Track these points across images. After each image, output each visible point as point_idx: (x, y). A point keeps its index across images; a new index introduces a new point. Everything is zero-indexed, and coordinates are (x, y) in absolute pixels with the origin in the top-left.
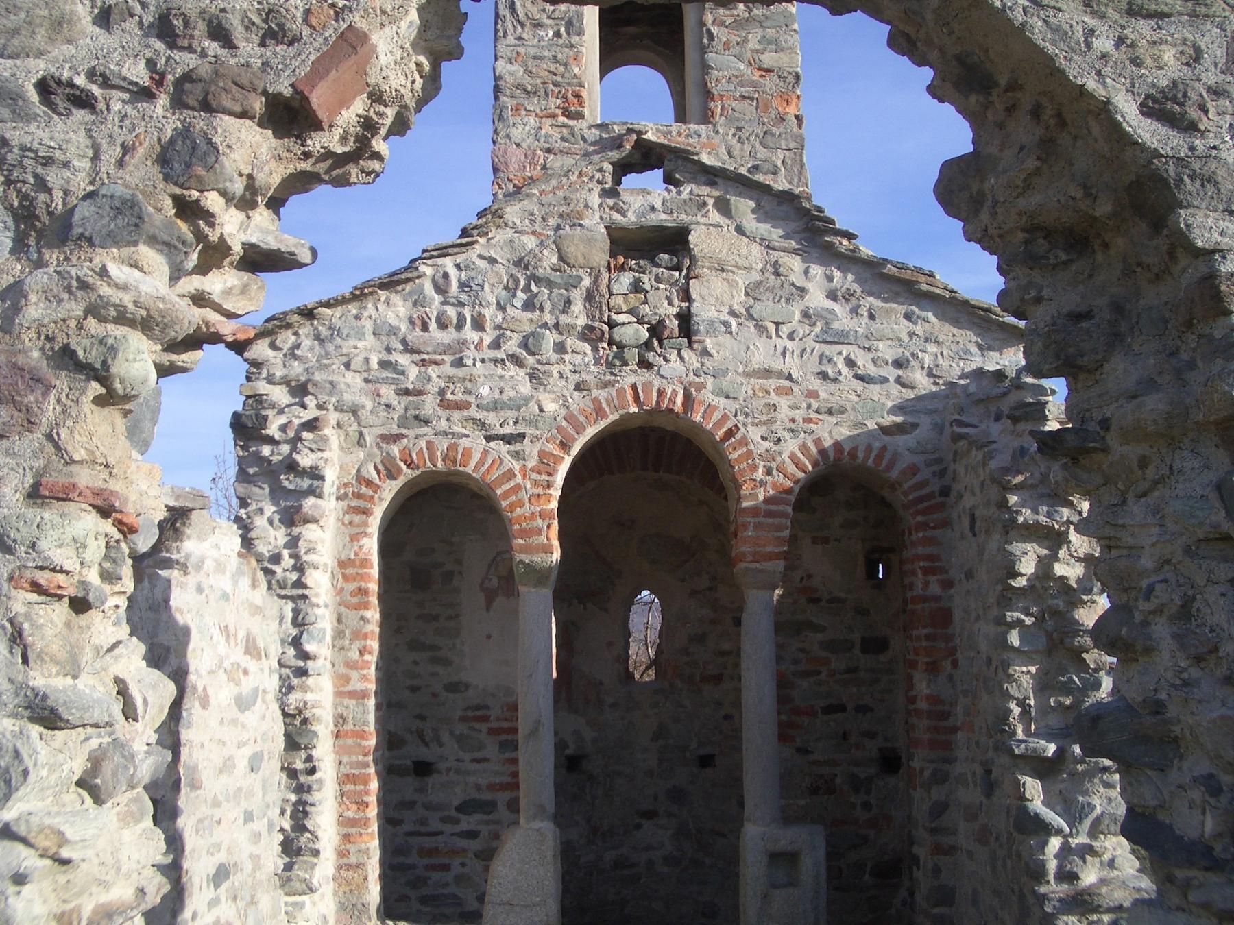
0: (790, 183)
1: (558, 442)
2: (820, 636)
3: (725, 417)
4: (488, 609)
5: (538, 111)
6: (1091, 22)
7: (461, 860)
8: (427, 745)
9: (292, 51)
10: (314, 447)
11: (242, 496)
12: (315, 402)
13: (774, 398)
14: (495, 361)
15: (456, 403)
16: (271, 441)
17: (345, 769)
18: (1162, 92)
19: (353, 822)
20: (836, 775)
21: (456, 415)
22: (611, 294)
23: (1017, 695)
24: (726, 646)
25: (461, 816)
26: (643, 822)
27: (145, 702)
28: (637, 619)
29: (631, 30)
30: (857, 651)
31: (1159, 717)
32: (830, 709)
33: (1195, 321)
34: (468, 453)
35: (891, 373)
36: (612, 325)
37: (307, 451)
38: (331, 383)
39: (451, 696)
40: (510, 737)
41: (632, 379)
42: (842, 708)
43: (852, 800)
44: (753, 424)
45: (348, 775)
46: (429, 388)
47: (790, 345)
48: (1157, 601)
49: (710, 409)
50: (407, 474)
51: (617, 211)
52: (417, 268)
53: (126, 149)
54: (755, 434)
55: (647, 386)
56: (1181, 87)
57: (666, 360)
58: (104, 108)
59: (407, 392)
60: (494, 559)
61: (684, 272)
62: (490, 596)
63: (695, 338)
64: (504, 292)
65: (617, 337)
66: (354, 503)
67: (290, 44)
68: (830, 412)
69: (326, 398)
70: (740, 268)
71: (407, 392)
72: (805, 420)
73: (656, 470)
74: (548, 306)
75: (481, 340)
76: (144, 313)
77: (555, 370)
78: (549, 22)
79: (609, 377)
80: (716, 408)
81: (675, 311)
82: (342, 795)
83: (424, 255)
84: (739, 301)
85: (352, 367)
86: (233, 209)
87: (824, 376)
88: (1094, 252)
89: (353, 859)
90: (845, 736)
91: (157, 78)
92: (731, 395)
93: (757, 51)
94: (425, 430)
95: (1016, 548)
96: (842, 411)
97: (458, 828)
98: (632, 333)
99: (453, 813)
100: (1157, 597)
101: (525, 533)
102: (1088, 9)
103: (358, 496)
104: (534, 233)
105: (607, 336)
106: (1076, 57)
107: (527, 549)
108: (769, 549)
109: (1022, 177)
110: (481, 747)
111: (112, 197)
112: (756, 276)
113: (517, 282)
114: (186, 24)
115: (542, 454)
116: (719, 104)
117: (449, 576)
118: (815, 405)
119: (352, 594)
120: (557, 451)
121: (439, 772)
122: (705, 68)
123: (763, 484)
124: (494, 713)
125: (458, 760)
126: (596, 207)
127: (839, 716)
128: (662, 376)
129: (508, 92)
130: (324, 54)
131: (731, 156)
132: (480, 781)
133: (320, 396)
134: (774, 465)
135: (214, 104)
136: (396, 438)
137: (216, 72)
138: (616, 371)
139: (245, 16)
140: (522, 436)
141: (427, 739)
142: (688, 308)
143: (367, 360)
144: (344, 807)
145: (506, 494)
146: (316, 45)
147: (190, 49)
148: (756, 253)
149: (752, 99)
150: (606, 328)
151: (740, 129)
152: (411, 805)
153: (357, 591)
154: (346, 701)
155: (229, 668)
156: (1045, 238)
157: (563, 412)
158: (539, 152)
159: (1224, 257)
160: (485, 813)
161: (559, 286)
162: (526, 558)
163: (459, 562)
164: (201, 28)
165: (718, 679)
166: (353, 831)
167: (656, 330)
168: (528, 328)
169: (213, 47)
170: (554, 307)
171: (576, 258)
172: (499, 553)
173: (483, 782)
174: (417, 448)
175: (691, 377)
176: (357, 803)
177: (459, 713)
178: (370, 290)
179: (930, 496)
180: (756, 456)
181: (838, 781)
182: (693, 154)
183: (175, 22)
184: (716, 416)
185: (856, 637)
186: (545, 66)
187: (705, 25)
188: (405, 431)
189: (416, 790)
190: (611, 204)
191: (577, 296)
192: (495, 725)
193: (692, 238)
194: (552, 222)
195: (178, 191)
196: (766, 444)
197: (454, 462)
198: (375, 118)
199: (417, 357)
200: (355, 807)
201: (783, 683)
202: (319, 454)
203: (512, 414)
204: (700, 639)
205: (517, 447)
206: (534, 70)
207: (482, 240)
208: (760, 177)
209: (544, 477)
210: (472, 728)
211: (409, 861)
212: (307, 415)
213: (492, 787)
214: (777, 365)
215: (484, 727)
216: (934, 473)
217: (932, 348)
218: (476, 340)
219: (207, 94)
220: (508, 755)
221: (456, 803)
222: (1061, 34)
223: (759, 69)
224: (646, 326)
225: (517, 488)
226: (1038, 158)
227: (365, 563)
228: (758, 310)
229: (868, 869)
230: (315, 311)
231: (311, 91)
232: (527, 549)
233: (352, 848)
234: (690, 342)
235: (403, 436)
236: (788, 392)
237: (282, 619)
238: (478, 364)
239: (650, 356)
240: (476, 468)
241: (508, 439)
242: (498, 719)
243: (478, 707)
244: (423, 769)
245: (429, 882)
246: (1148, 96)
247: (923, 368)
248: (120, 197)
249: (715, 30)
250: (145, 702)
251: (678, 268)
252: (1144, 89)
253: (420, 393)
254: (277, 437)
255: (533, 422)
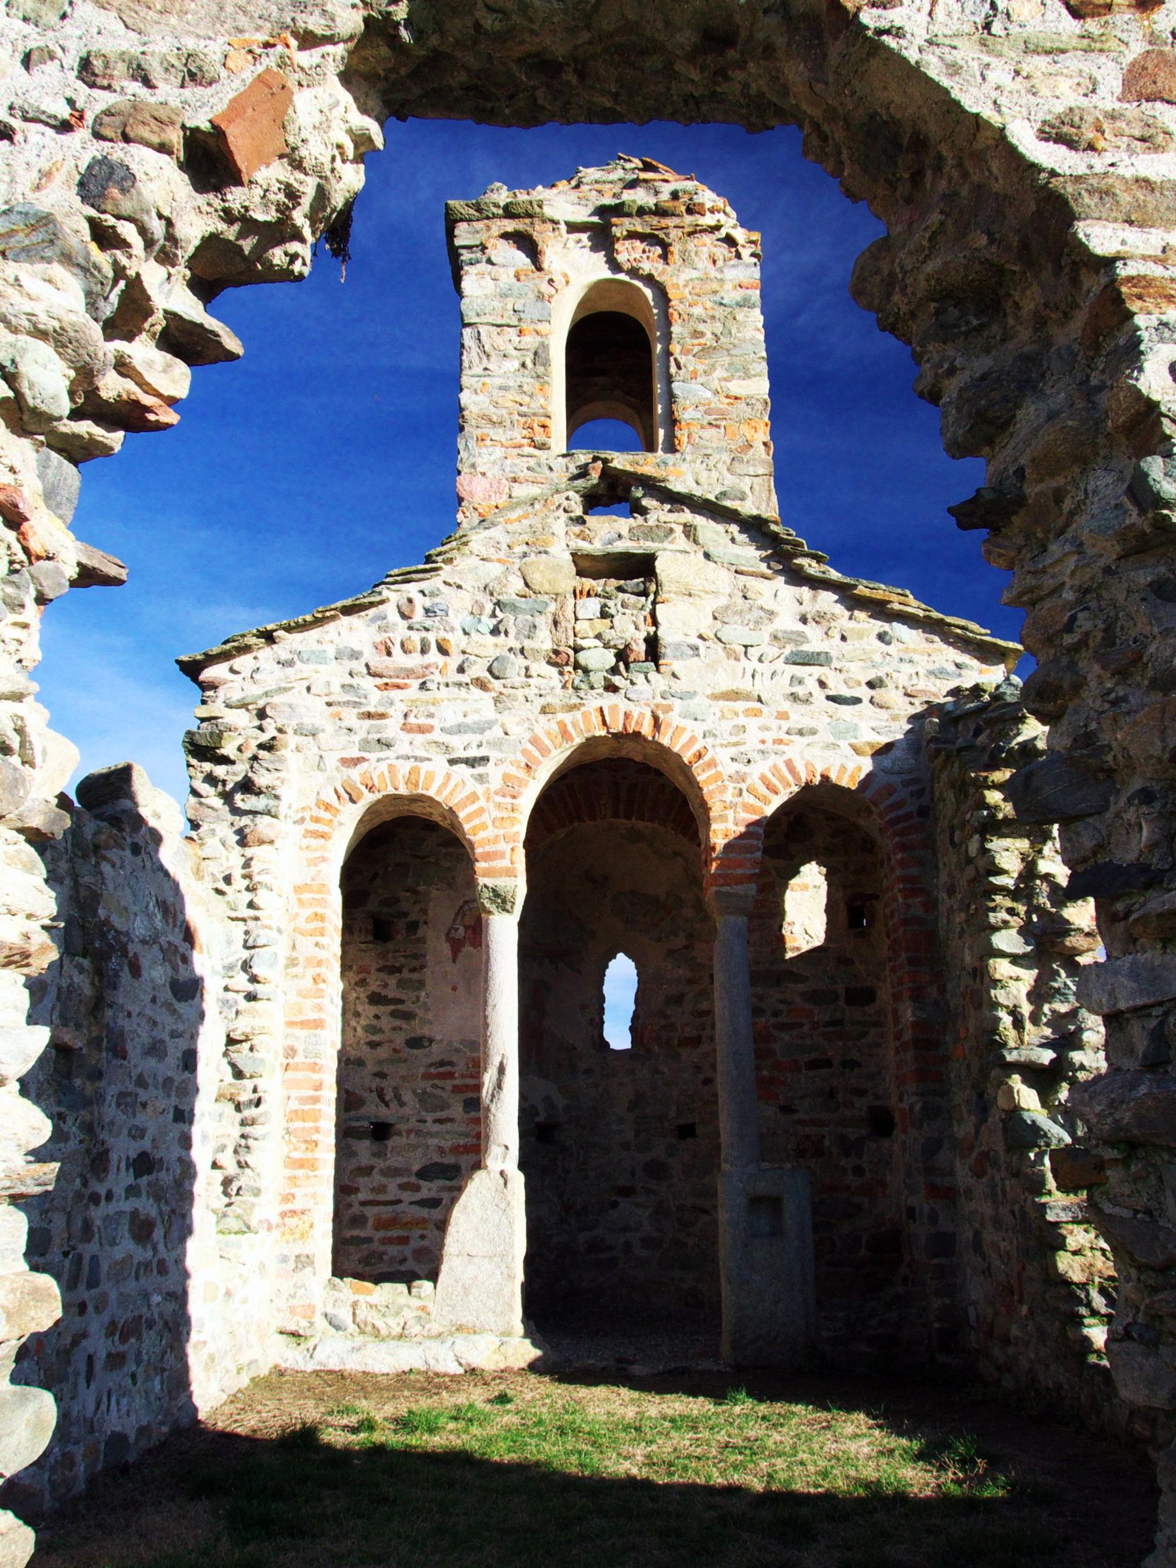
0: (758, 508)
1: (523, 765)
2: (801, 987)
3: (693, 739)
4: (454, 961)
5: (504, 441)
6: (986, 59)
7: (421, 1232)
8: (387, 1105)
9: (210, 91)
10: (271, 767)
11: (193, 818)
12: (274, 725)
13: (742, 720)
14: (459, 685)
15: (419, 726)
16: (226, 760)
17: (294, 1105)
18: (1059, 117)
19: (300, 1164)
20: (824, 1136)
21: (419, 738)
22: (577, 619)
23: (1006, 1003)
24: (704, 1006)
25: (421, 1182)
26: (619, 1199)
27: (44, 752)
28: (609, 988)
29: (601, 380)
30: (841, 1003)
31: (1028, 471)
32: (813, 1065)
33: (1101, 338)
34: (430, 776)
35: (864, 693)
36: (577, 649)
37: (264, 771)
38: (290, 706)
39: (415, 1051)
40: (471, 1095)
41: (598, 703)
42: (828, 1063)
43: (843, 1163)
44: (722, 745)
45: (296, 1111)
46: (390, 711)
47: (759, 666)
48: (1079, 630)
49: (679, 730)
50: (368, 799)
51: (584, 539)
52: (380, 593)
53: (47, 175)
54: (723, 756)
55: (614, 708)
56: (1077, 111)
57: (632, 683)
58: (22, 140)
59: (369, 716)
60: (461, 908)
61: (651, 597)
62: (456, 947)
63: (661, 662)
64: (470, 618)
65: (582, 662)
66: (313, 827)
67: (210, 84)
68: (801, 733)
69: (285, 721)
70: (706, 592)
71: (369, 716)
72: (775, 742)
73: (628, 817)
74: (512, 631)
75: (445, 665)
76: (57, 325)
77: (520, 693)
78: (515, 353)
79: (577, 701)
80: (683, 729)
81: (643, 635)
82: (288, 1132)
83: (388, 580)
84: (706, 625)
85: (312, 691)
86: (152, 261)
87: (794, 697)
88: (1005, 316)
89: (297, 1205)
90: (832, 1094)
91: (77, 114)
92: (699, 717)
93: (725, 380)
94: (386, 753)
95: (996, 844)
96: (813, 732)
97: (418, 1196)
98: (599, 659)
99: (413, 1179)
100: (1080, 627)
101: (488, 856)
102: (984, 49)
103: (317, 820)
104: (499, 561)
105: (572, 659)
106: (971, 89)
107: (489, 873)
108: (740, 871)
109: (927, 235)
110: (444, 1106)
111: (27, 214)
112: (723, 601)
113: (482, 608)
114: (107, 66)
115: (506, 777)
116: (685, 432)
117: (413, 927)
118: (785, 727)
119: (309, 920)
120: (522, 774)
121: (399, 1134)
122: (671, 397)
123: (733, 806)
124: (459, 1070)
125: (419, 1121)
126: (562, 534)
127: (824, 1071)
128: (629, 699)
129: (473, 422)
130: (241, 94)
131: (697, 483)
132: (442, 1143)
133: (278, 720)
134: (744, 786)
135: (132, 135)
136: (357, 761)
137: (135, 107)
138: (582, 694)
139: (163, 59)
140: (485, 760)
141: (387, 1098)
142: (655, 632)
143: (328, 683)
144: (291, 1147)
145: (469, 818)
146: (234, 85)
147: (109, 88)
148: (723, 579)
149: (718, 427)
150: (571, 652)
151: (708, 456)
152: (367, 1171)
153: (313, 916)
154: (298, 1031)
155: (165, 946)
156: (955, 307)
157: (528, 735)
158: (504, 481)
159: (1125, 264)
160: (447, 1179)
161: (523, 611)
162: (490, 882)
163: (424, 911)
164: (120, 69)
165: (696, 1041)
166: (300, 1173)
167: (623, 655)
168: (493, 653)
169: (136, 87)
170: (518, 633)
171: (542, 584)
172: (466, 902)
173: (447, 1144)
174: (378, 772)
175: (659, 700)
176: (306, 1141)
177: (422, 1070)
178: (332, 613)
179: (909, 816)
180: (725, 777)
181: (827, 1143)
182: (660, 481)
183: (95, 62)
184: (684, 738)
185: (840, 988)
186: (511, 397)
187: (672, 354)
188: (366, 755)
189: (374, 1155)
190: (578, 532)
191: (544, 622)
192: (457, 1082)
193: (659, 565)
194: (519, 549)
195: (93, 213)
196: (736, 766)
197: (416, 785)
198: (296, 185)
199: (379, 681)
200: (303, 1146)
201: (761, 1039)
202: (277, 774)
203: (475, 738)
204: (678, 1000)
205: (479, 770)
206: (500, 401)
207: (447, 568)
208: (728, 503)
209: (509, 800)
210: (435, 1086)
211: (362, 1233)
212: (264, 738)
213: (455, 1149)
214: (745, 685)
215: (448, 1084)
216: (912, 794)
217: (907, 669)
218: (441, 665)
219: (125, 126)
220: (473, 1114)
221: (416, 1167)
222: (954, 69)
223: (728, 397)
224: (613, 651)
225: (481, 811)
226: (942, 212)
227: (322, 888)
228: (726, 633)
229: (864, 1242)
230: (275, 634)
231: (228, 127)
232: (489, 873)
233: (298, 1192)
234: (657, 666)
235: (364, 759)
236: (757, 714)
237: (229, 942)
238: (442, 687)
239: (617, 680)
240: (439, 792)
241: (471, 762)
242: (463, 1076)
243: (442, 1064)
244: (381, 1131)
245: (385, 1257)
246: (1044, 122)
247: (897, 687)
248: (35, 214)
249: (682, 360)
250: (44, 752)
251: (644, 593)
252: (1041, 116)
253: (382, 716)
254: (232, 757)
255: (496, 744)
